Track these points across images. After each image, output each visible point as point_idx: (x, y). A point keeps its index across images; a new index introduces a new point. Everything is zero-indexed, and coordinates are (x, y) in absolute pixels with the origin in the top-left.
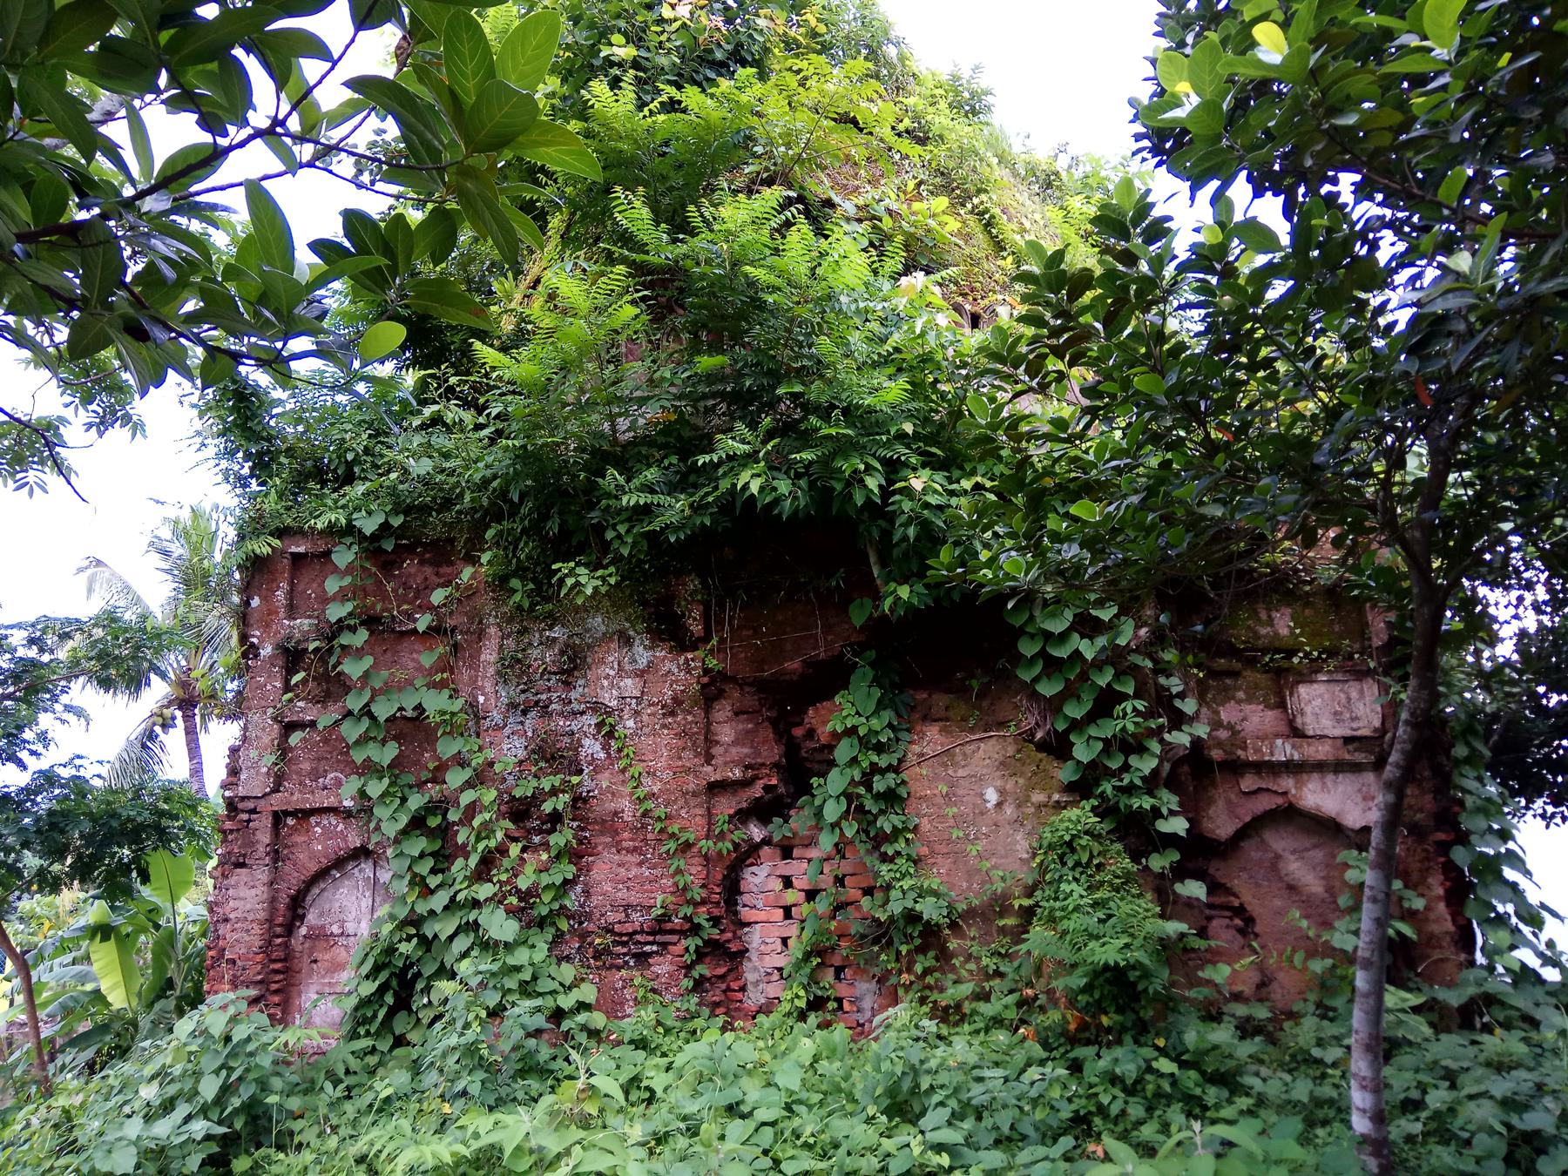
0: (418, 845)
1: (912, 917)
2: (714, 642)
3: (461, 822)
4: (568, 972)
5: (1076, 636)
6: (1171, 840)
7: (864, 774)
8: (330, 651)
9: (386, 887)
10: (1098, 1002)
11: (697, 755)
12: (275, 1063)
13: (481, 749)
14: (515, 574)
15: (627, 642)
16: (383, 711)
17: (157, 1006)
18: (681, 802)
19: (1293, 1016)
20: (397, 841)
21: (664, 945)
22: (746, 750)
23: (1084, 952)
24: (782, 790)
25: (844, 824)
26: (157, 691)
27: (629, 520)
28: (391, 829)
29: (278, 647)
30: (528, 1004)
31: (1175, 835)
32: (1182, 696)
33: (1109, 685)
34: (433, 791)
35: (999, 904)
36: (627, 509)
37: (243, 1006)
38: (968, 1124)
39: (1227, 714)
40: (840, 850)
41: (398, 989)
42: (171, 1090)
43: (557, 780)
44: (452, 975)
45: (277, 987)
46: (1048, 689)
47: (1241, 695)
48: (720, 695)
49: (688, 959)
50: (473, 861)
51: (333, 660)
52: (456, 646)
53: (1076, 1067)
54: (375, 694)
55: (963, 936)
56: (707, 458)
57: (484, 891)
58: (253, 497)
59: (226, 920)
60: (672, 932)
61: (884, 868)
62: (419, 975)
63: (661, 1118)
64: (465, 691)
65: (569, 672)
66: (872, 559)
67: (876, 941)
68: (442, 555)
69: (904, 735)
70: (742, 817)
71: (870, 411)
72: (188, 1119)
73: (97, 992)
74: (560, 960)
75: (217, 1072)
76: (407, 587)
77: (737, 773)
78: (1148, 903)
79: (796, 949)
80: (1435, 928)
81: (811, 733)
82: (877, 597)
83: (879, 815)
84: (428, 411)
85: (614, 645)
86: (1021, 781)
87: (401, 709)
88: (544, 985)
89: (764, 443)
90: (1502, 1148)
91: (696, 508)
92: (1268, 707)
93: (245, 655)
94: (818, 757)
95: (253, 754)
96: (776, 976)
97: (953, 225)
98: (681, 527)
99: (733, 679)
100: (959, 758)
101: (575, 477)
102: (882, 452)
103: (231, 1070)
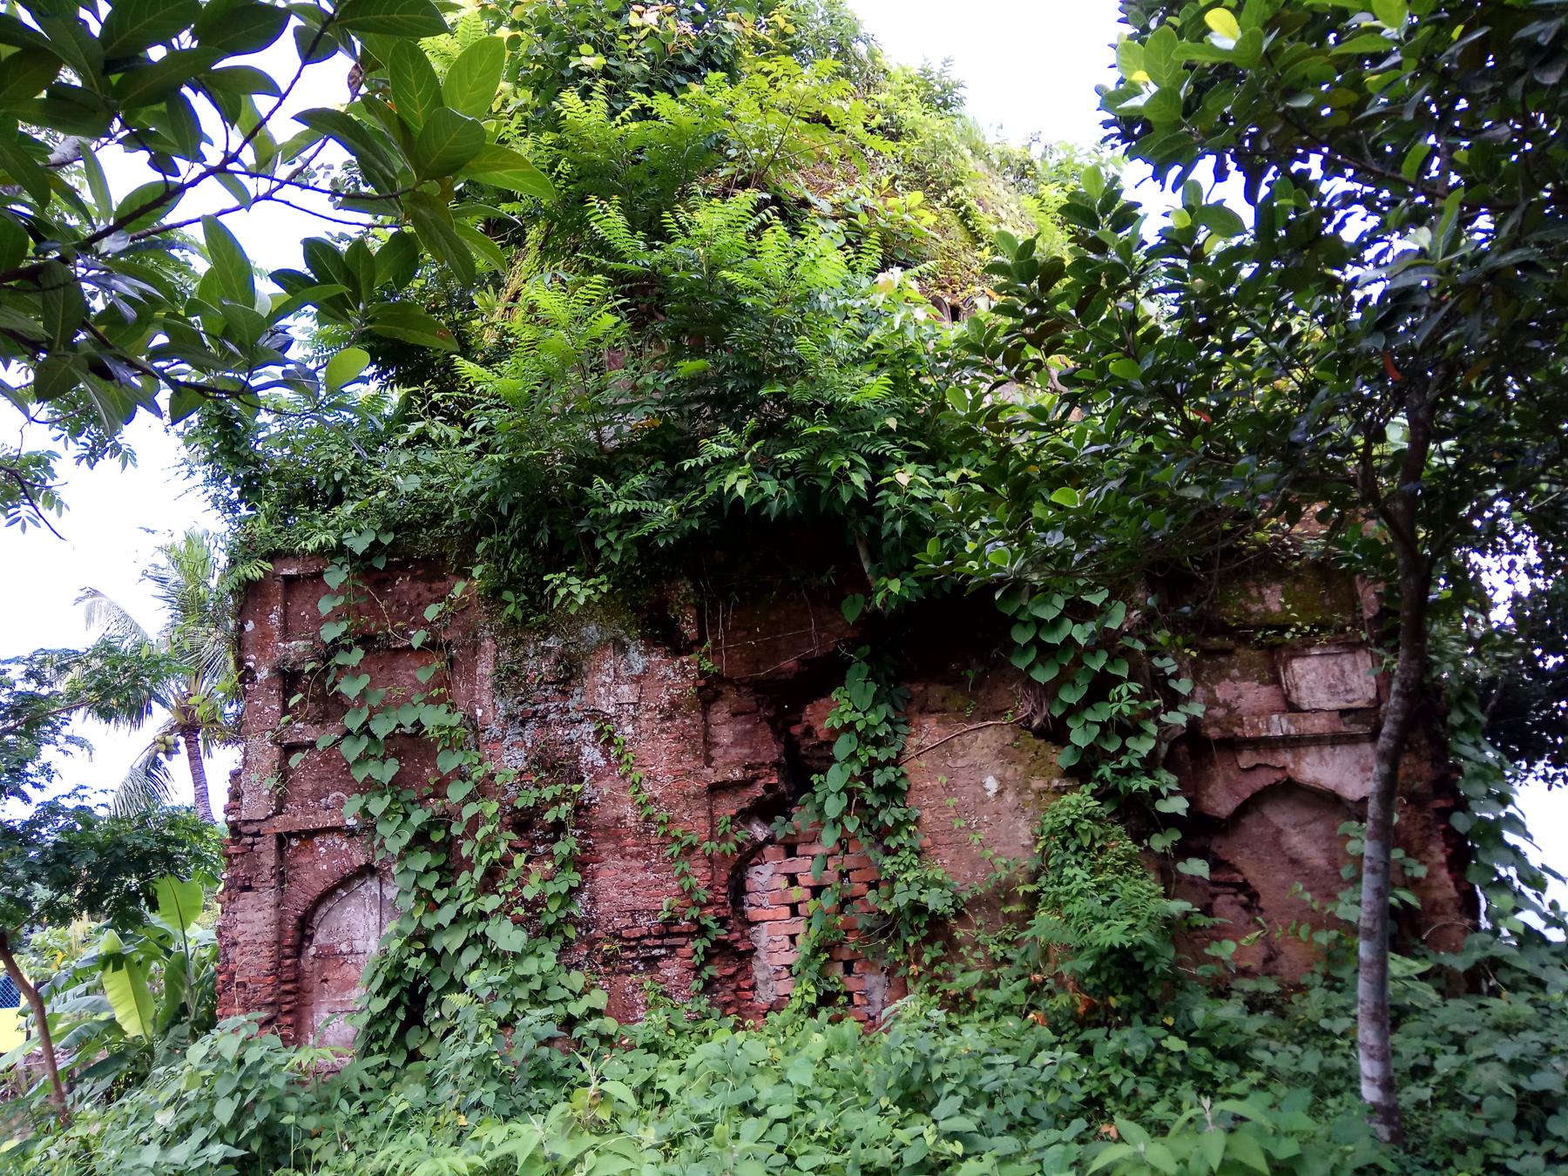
0: (422, 860)
1: (917, 908)
2: (709, 644)
3: (464, 836)
4: (577, 979)
5: (1068, 622)
6: (1171, 820)
7: (864, 769)
8: (327, 671)
9: (393, 903)
10: (1106, 983)
11: (697, 758)
12: (290, 1083)
13: (481, 762)
14: (507, 587)
15: (622, 648)
16: (381, 728)
17: (172, 1032)
18: (682, 806)
19: (1301, 989)
20: (401, 857)
21: (672, 948)
22: (746, 751)
23: (1089, 935)
24: (783, 788)
25: (846, 819)
26: (159, 718)
27: (618, 527)
28: (394, 846)
29: (274, 669)
30: (539, 1013)
31: (1175, 814)
32: (1176, 676)
33: (1103, 669)
34: (436, 805)
35: (1004, 892)
36: (616, 516)
37: (255, 1028)
38: (980, 1112)
39: (1222, 692)
40: (843, 845)
41: (409, 1004)
42: (188, 1115)
43: (558, 790)
44: (462, 988)
45: (288, 1008)
46: (1043, 676)
47: (1235, 672)
48: (718, 696)
49: (696, 960)
50: (478, 873)
51: (329, 681)
52: (452, 661)
53: (1086, 1050)
54: (373, 712)
55: (969, 925)
56: (693, 462)
57: (491, 903)
58: (242, 522)
59: (235, 944)
60: (680, 934)
61: (888, 861)
62: (429, 989)
63: (675, 1119)
64: (463, 704)
65: (565, 681)
66: (863, 555)
67: (884, 934)
68: (433, 570)
69: (902, 729)
70: (744, 817)
71: (854, 408)
72: (205, 1143)
73: (112, 1021)
74: (569, 968)
75: (231, 1095)
76: (400, 604)
77: (738, 774)
78: (1152, 884)
79: (804, 946)
80: (1438, 895)
81: (809, 731)
82: (869, 593)
83: (880, 809)
84: (413, 428)
85: (610, 652)
86: (1020, 768)
87: (400, 726)
88: (554, 993)
89: (749, 444)
90: (1512, 1112)
91: (685, 512)
92: (1263, 683)
93: (242, 680)
94: (818, 753)
95: (255, 777)
96: (785, 973)
97: (929, 219)
98: (669, 531)
99: (729, 681)
100: (957, 748)
101: (563, 487)
102: (867, 449)
103: (245, 1092)
